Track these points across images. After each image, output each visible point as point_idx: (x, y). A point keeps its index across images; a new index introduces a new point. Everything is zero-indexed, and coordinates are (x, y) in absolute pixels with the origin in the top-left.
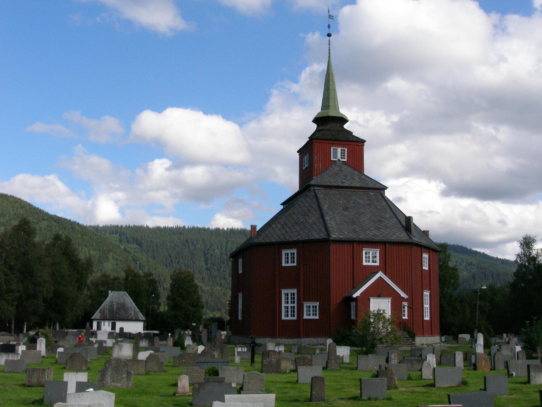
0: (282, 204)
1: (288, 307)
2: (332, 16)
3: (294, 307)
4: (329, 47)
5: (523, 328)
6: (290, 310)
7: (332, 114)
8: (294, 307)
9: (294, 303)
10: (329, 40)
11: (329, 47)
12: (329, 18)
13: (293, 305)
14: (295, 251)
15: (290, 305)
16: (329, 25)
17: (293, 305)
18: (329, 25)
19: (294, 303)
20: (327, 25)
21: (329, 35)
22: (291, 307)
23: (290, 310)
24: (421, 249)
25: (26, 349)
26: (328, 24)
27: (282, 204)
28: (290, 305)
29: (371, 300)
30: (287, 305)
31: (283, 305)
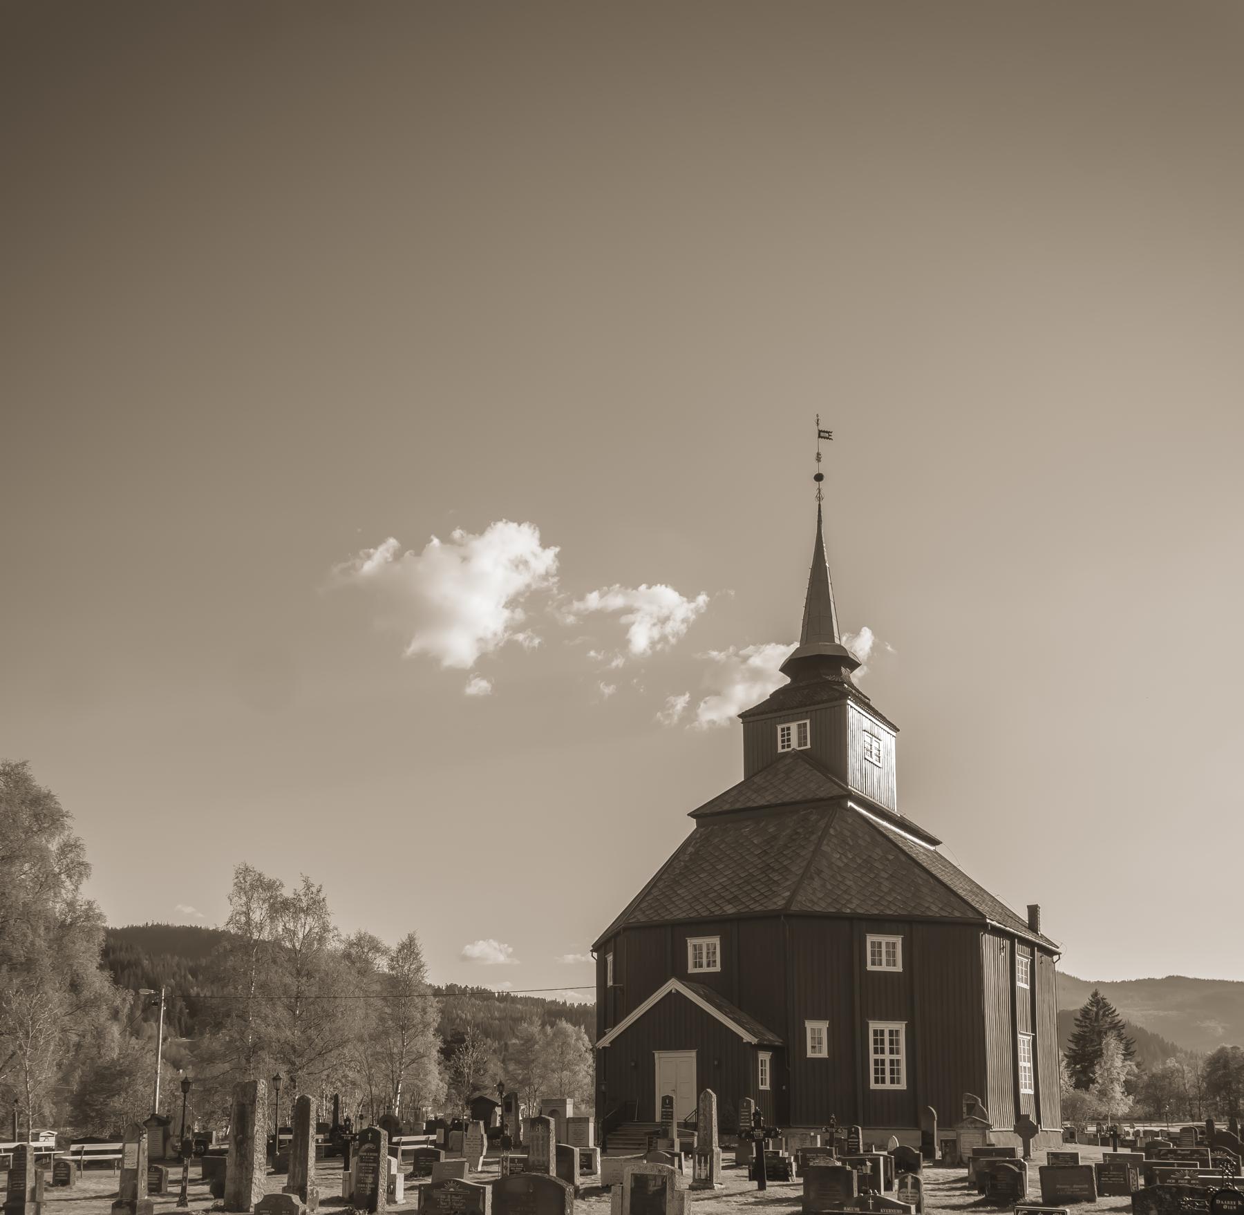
0: (692, 815)
1: (892, 1052)
2: (827, 432)
3: (876, 1052)
4: (819, 505)
5: (561, 1020)
6: (887, 1046)
7: (823, 649)
8: (876, 1052)
9: (876, 1062)
10: (818, 421)
11: (819, 505)
12: (819, 436)
13: (880, 1057)
14: (716, 940)
15: (887, 1057)
16: (818, 454)
17: (880, 1057)
18: (818, 454)
19: (876, 1062)
20: (815, 456)
21: (819, 478)
22: (883, 1052)
23: (887, 1046)
24: (1032, 954)
25: (180, 1166)
26: (816, 452)
27: (692, 815)
28: (887, 1057)
29: (656, 1055)
30: (895, 1057)
31: (902, 1057)
